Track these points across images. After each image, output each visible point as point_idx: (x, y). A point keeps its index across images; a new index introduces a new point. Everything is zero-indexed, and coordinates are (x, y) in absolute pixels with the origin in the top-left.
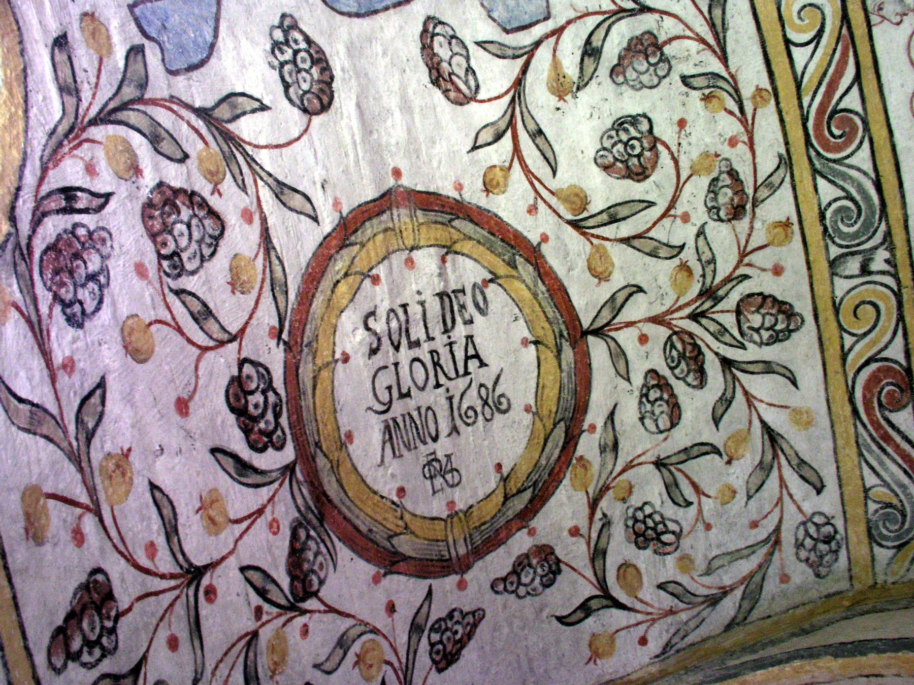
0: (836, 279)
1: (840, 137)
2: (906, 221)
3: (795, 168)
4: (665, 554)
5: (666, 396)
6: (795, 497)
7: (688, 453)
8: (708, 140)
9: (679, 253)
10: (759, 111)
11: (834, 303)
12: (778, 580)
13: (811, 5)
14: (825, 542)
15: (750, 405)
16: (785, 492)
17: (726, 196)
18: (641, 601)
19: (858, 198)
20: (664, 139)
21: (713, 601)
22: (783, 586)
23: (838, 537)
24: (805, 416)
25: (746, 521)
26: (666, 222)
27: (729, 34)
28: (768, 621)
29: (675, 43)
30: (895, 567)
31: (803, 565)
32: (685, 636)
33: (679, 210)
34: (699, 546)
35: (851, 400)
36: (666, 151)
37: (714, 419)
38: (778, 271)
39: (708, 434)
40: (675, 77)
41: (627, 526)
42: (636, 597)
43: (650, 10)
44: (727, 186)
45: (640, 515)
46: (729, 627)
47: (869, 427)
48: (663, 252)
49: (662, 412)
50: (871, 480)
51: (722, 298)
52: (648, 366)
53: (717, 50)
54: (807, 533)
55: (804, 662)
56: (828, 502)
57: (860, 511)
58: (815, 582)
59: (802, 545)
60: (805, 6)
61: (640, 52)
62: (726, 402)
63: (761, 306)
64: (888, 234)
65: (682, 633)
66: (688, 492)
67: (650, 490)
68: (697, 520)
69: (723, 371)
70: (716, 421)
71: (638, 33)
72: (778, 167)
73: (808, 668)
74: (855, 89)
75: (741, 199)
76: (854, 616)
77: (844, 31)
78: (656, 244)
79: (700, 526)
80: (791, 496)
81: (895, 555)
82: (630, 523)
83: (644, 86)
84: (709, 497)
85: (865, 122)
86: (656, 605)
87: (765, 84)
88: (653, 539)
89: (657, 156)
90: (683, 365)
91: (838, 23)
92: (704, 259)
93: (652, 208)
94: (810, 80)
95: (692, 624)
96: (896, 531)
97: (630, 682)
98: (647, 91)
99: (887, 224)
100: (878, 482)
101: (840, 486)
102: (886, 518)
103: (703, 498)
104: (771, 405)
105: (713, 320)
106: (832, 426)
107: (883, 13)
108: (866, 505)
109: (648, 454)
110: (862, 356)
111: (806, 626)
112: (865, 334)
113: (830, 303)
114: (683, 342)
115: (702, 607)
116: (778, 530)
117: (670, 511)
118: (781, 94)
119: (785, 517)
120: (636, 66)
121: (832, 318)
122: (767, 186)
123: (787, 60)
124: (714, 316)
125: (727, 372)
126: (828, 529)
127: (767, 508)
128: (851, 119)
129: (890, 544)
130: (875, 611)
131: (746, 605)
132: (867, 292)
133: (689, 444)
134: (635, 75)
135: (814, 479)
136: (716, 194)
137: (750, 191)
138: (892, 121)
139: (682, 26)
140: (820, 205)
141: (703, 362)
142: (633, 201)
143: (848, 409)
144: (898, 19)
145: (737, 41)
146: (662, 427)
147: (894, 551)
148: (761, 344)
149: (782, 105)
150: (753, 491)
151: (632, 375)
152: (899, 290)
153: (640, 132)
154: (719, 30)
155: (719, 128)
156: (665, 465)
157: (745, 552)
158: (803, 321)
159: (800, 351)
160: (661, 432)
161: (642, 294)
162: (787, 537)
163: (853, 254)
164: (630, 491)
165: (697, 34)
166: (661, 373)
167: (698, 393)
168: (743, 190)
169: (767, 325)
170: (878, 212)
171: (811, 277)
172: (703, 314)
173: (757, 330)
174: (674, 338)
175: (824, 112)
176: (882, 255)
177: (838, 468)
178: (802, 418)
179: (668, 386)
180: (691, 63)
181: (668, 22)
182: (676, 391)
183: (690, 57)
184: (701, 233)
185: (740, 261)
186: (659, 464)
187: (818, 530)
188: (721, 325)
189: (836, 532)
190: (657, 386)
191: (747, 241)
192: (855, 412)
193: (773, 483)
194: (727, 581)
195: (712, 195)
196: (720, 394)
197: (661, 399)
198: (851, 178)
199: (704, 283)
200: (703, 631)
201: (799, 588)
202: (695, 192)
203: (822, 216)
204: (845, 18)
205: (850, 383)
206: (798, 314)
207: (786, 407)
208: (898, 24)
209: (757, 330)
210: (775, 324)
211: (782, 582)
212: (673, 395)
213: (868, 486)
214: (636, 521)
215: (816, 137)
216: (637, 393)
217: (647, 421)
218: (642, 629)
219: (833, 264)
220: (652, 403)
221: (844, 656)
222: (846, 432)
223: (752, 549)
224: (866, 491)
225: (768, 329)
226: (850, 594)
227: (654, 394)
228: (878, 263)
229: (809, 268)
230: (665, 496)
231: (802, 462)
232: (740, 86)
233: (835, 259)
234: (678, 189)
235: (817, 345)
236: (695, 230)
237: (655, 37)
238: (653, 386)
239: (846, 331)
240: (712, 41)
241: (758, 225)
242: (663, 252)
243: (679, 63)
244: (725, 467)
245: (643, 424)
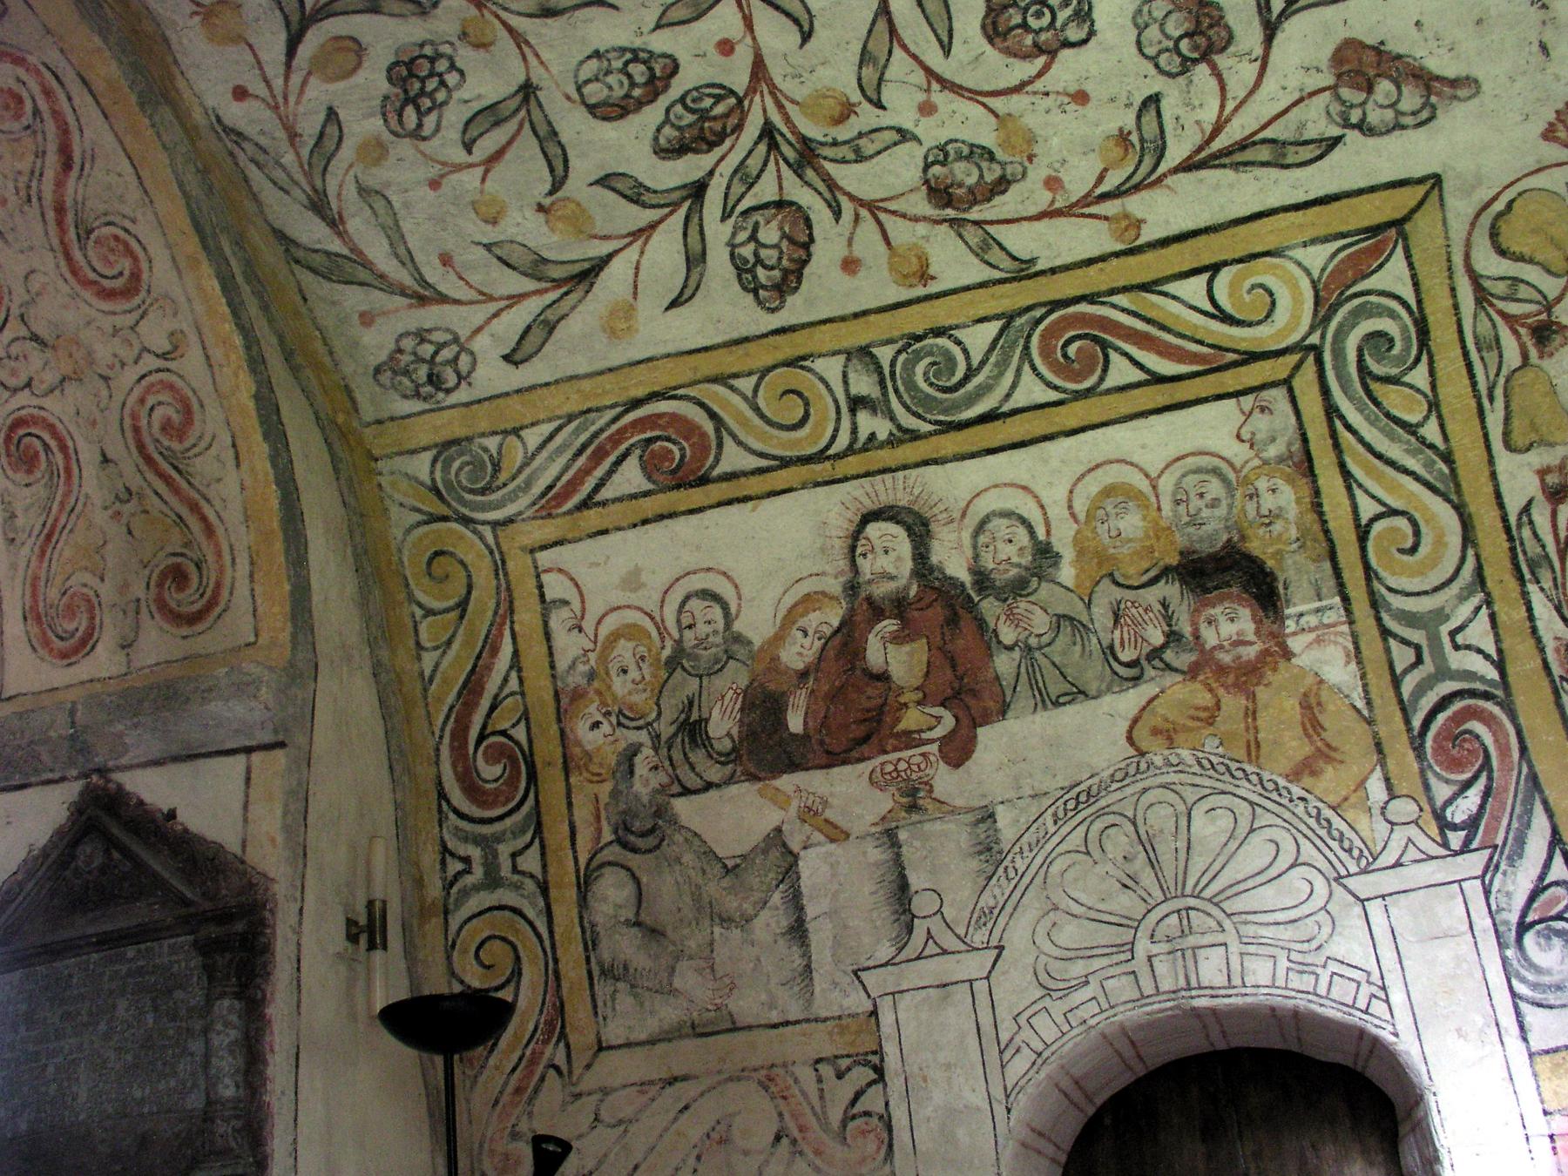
0: (842, 358)
1: (1065, 356)
2: (936, 462)
3: (1015, 284)
4: (384, 114)
5: (637, 92)
6: (495, 321)
7: (548, 138)
8: (1055, 141)
9: (870, 101)
10: (1104, 225)
11: (804, 358)
12: (364, 308)
13: (1273, 303)
14: (430, 376)
15: (636, 234)
16: (502, 304)
17: (966, 174)
18: (304, 83)
19: (970, 386)
20: (1055, 66)
21: (319, 205)
22: (356, 317)
23: (441, 395)
24: (624, 326)
25: (450, 246)
26: (919, 77)
27: (1228, 175)
28: (298, 298)
29: (1213, 83)
30: (404, 484)
31: (392, 346)
32: (257, 164)
33: (939, 97)
34: (403, 172)
35: (654, 396)
36: (1034, 72)
37: (608, 176)
38: (850, 265)
39: (583, 169)
40: (1157, 84)
41: (422, 45)
42: (309, 73)
43: (1269, 39)
44: (981, 176)
45: (442, 66)
46: (281, 236)
47: (615, 427)
48: (869, 73)
49: (610, 88)
50: (533, 437)
51: (800, 177)
52: (683, 58)
53: (1203, 155)
54: (440, 347)
55: (241, 351)
56: (492, 375)
57: (484, 426)
58: (366, 367)
59: (423, 341)
60: (1271, 294)
61: (1198, 23)
62: (637, 194)
63: (792, 241)
64: (915, 436)
65: (261, 158)
66: (488, 144)
67: (485, 80)
68: (444, 164)
69: (685, 186)
70: (605, 181)
71: (1230, 19)
72: (1015, 258)
73: (233, 357)
74: (1143, 376)
75: (961, 200)
76: (322, 429)
77: (1231, 357)
78: (882, 61)
79: (435, 171)
80: (496, 315)
81: (422, 484)
82: (428, 50)
83: (1141, 29)
84: (483, 180)
85: (1088, 393)
86: (301, 109)
87: (1148, 234)
88: (406, 91)
89: (1026, 57)
90: (689, 118)
91: (1243, 346)
92: (862, 142)
93: (940, 52)
94: (1153, 305)
95: (279, 174)
96: (459, 482)
97: (172, 79)
98: (1134, 38)
99: (931, 434)
100: (531, 447)
101: (518, 391)
102: (477, 465)
103: (480, 171)
104: (637, 268)
105: (765, 164)
106: (610, 370)
107: (1256, 412)
108: (495, 433)
109: (542, 70)
110: (723, 408)
111: (299, 360)
112: (757, 410)
113: (802, 352)
114: (727, 115)
115: (308, 189)
116: (443, 299)
117: (455, 116)
118: (1131, 260)
119: (462, 308)
120: (1174, 17)
121: (779, 357)
122: (984, 241)
123: (1186, 268)
124: (771, 166)
125: (684, 193)
126: (451, 380)
127: (475, 279)
128: (1091, 372)
129: (438, 475)
130: (335, 461)
131: (318, 260)
132: (823, 407)
133: (564, 139)
134: (1159, 14)
135: (528, 347)
136: (968, 158)
137: (974, 214)
138: (1090, 433)
139: (1242, 94)
140: (957, 327)
141: (696, 151)
142: (950, 18)
143: (640, 392)
144: (1246, 436)
145: (1217, 187)
146: (586, 90)
147: (429, 482)
148: (732, 246)
149: (1115, 262)
150: (499, 252)
151: (667, 32)
152: (828, 458)
153: (1065, 25)
154: (1235, 156)
155: (1074, 160)
156: (526, 100)
157: (402, 251)
158: (773, 310)
159: (726, 310)
160: (579, 89)
161: (799, 41)
162: (431, 316)
163: (882, 383)
164: (479, 46)
165: (1228, 120)
166: (675, 81)
167: (647, 148)
168: (975, 202)
169: (764, 253)
170: (949, 419)
171: (843, 319)
172: (773, 146)
173: (753, 237)
174: (733, 101)
175: (1104, 330)
176: (883, 429)
177: (547, 384)
178: (620, 320)
179: (653, 97)
180: (1180, 112)
181: (1249, 71)
182: (647, 109)
183: (1192, 109)
184: (904, 135)
185: (861, 203)
186: (527, 90)
187: (448, 362)
188: (758, 177)
189: (448, 391)
190: (652, 78)
191: (894, 213)
192: (636, 403)
193: (516, 283)
194: (354, 225)
195: (966, 150)
196: (648, 183)
197: (633, 85)
198: (1001, 374)
199: (822, 144)
200: (269, 194)
201: (356, 344)
202: (966, 123)
203: (939, 332)
204: (1252, 357)
205: (680, 392)
206: (783, 302)
207: (635, 294)
208: (1238, 436)
209: (753, 237)
210: (765, 267)
211: (362, 315)
212: (640, 104)
213: (522, 433)
214: (432, 60)
215: (1063, 318)
216: (638, 43)
217: (594, 64)
218: (259, 88)
219: (865, 352)
220: (624, 71)
221: (258, 410)
222: (605, 393)
223: (408, 260)
224: (516, 431)
225: (756, 254)
226: (355, 424)
227: (638, 71)
228: (868, 423)
229: (856, 316)
230: (476, 106)
231: (551, 328)
232: (1144, 194)
233: (872, 356)
234: (974, 95)
235: (735, 335)
236: (908, 125)
237: (1224, 49)
238: (651, 69)
239: (761, 378)
240: (1217, 145)
241: (922, 229)
242: (869, 73)
243: (1181, 92)
244: (533, 201)
245: (589, 57)
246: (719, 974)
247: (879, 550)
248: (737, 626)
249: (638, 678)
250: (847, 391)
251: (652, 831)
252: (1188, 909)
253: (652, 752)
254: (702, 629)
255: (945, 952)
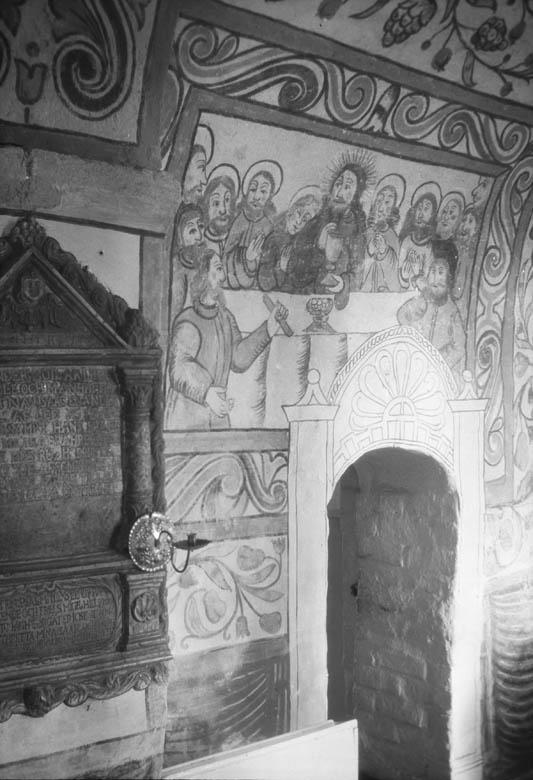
0: (389, 85)
152: (352, 129)
163: (393, 106)
173: (409, 9)
209: (409, 9)
225: (403, 16)
246: (228, 397)
247: (344, 185)
248: (274, 200)
249: (223, 212)
250: (379, 101)
251: (213, 307)
252: (405, 403)
253: (218, 259)
254: (259, 194)
255: (319, 404)
